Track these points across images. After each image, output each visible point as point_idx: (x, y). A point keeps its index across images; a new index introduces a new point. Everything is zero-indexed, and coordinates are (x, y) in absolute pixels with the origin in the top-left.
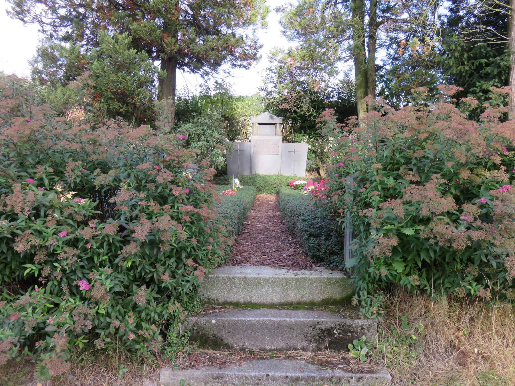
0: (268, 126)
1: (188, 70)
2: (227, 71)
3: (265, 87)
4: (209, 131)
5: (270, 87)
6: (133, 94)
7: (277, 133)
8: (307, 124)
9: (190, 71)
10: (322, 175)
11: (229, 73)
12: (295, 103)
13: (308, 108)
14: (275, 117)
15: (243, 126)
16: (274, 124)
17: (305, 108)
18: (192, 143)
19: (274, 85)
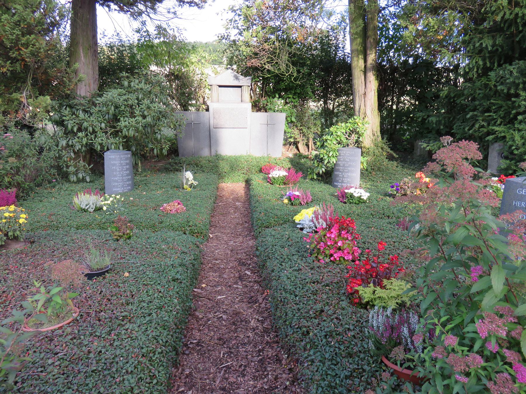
0: (212, 142)
1: (116, 7)
2: (172, 10)
3: (226, 35)
4: (146, 102)
5: (233, 34)
6: (16, 44)
7: (244, 98)
8: (282, 86)
9: (118, 9)
10: (301, 151)
11: (175, 13)
12: (268, 58)
13: (287, 65)
14: (241, 77)
15: (199, 87)
16: (240, 87)
17: (283, 67)
18: (122, 119)
19: (237, 31)
